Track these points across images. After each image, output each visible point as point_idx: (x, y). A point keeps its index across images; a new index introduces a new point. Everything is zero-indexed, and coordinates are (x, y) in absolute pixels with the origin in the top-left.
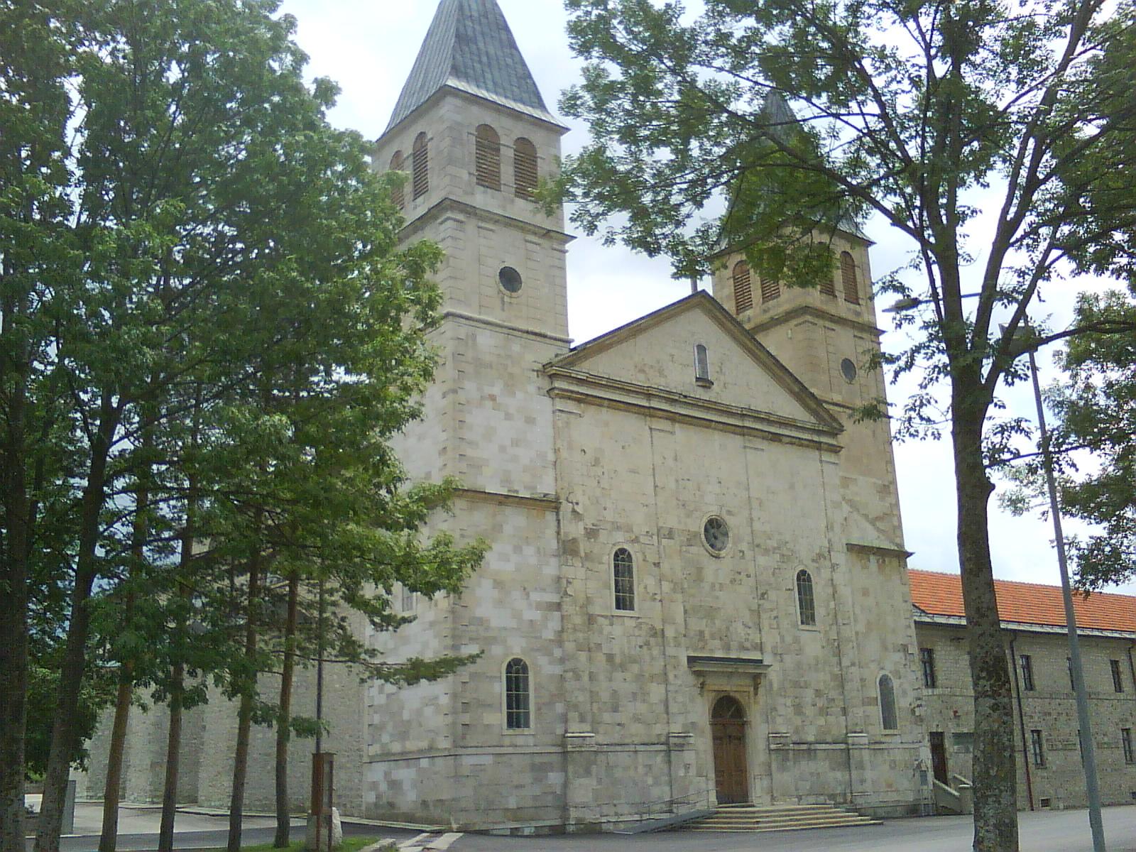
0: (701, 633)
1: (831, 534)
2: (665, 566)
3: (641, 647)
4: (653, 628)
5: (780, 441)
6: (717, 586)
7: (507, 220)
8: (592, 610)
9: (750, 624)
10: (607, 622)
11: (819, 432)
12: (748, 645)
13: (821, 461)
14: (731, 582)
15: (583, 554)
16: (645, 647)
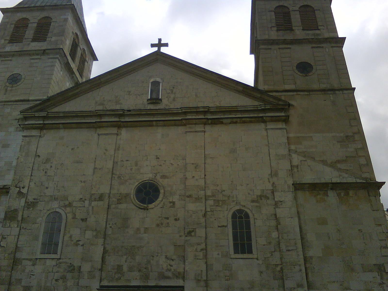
0: (119, 268)
1: (275, 179)
2: (92, 220)
3: (57, 280)
4: (71, 265)
5: (222, 123)
6: (142, 230)
7: (20, 53)
8: (18, 255)
9: (174, 257)
10: (30, 263)
11: (264, 111)
12: (170, 274)
13: (266, 130)
14: (158, 225)
15: (20, 218)
16: (61, 281)
